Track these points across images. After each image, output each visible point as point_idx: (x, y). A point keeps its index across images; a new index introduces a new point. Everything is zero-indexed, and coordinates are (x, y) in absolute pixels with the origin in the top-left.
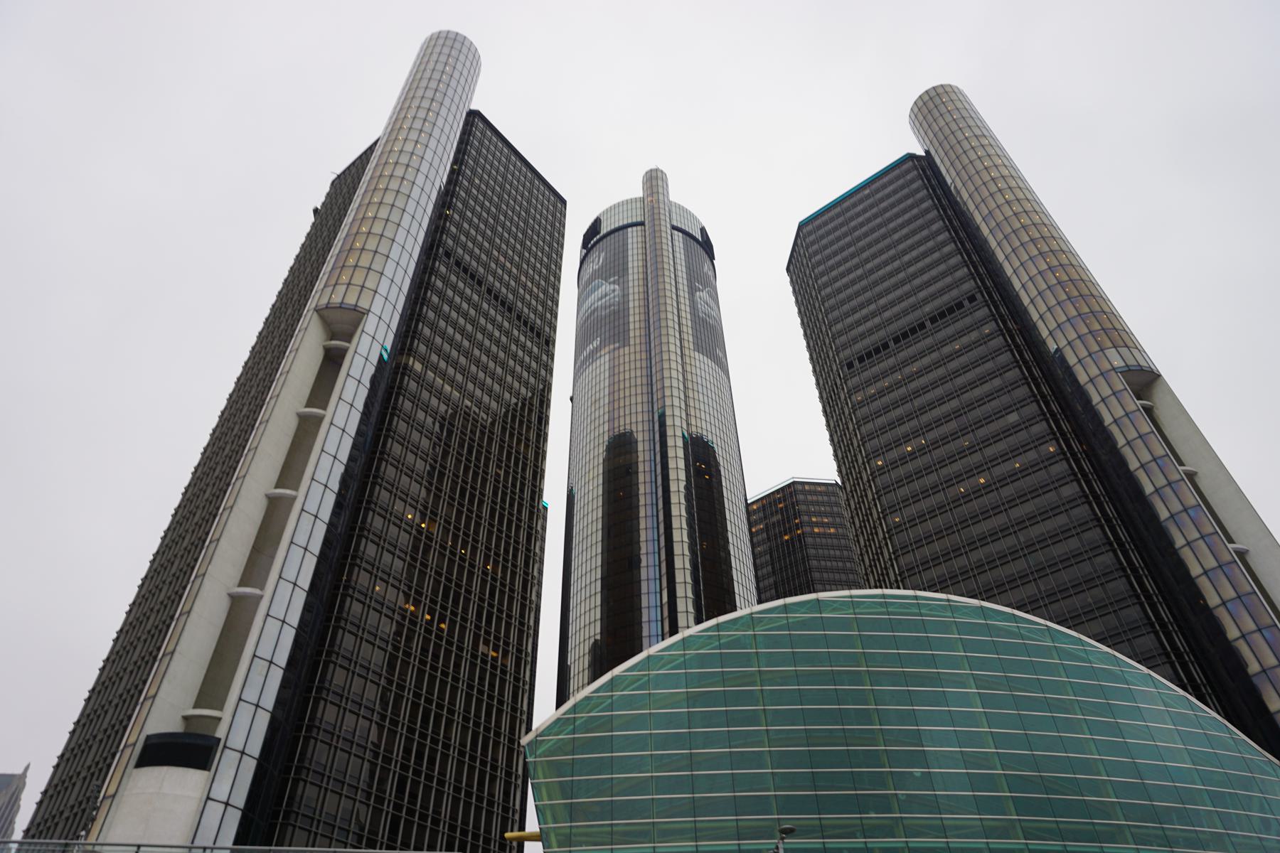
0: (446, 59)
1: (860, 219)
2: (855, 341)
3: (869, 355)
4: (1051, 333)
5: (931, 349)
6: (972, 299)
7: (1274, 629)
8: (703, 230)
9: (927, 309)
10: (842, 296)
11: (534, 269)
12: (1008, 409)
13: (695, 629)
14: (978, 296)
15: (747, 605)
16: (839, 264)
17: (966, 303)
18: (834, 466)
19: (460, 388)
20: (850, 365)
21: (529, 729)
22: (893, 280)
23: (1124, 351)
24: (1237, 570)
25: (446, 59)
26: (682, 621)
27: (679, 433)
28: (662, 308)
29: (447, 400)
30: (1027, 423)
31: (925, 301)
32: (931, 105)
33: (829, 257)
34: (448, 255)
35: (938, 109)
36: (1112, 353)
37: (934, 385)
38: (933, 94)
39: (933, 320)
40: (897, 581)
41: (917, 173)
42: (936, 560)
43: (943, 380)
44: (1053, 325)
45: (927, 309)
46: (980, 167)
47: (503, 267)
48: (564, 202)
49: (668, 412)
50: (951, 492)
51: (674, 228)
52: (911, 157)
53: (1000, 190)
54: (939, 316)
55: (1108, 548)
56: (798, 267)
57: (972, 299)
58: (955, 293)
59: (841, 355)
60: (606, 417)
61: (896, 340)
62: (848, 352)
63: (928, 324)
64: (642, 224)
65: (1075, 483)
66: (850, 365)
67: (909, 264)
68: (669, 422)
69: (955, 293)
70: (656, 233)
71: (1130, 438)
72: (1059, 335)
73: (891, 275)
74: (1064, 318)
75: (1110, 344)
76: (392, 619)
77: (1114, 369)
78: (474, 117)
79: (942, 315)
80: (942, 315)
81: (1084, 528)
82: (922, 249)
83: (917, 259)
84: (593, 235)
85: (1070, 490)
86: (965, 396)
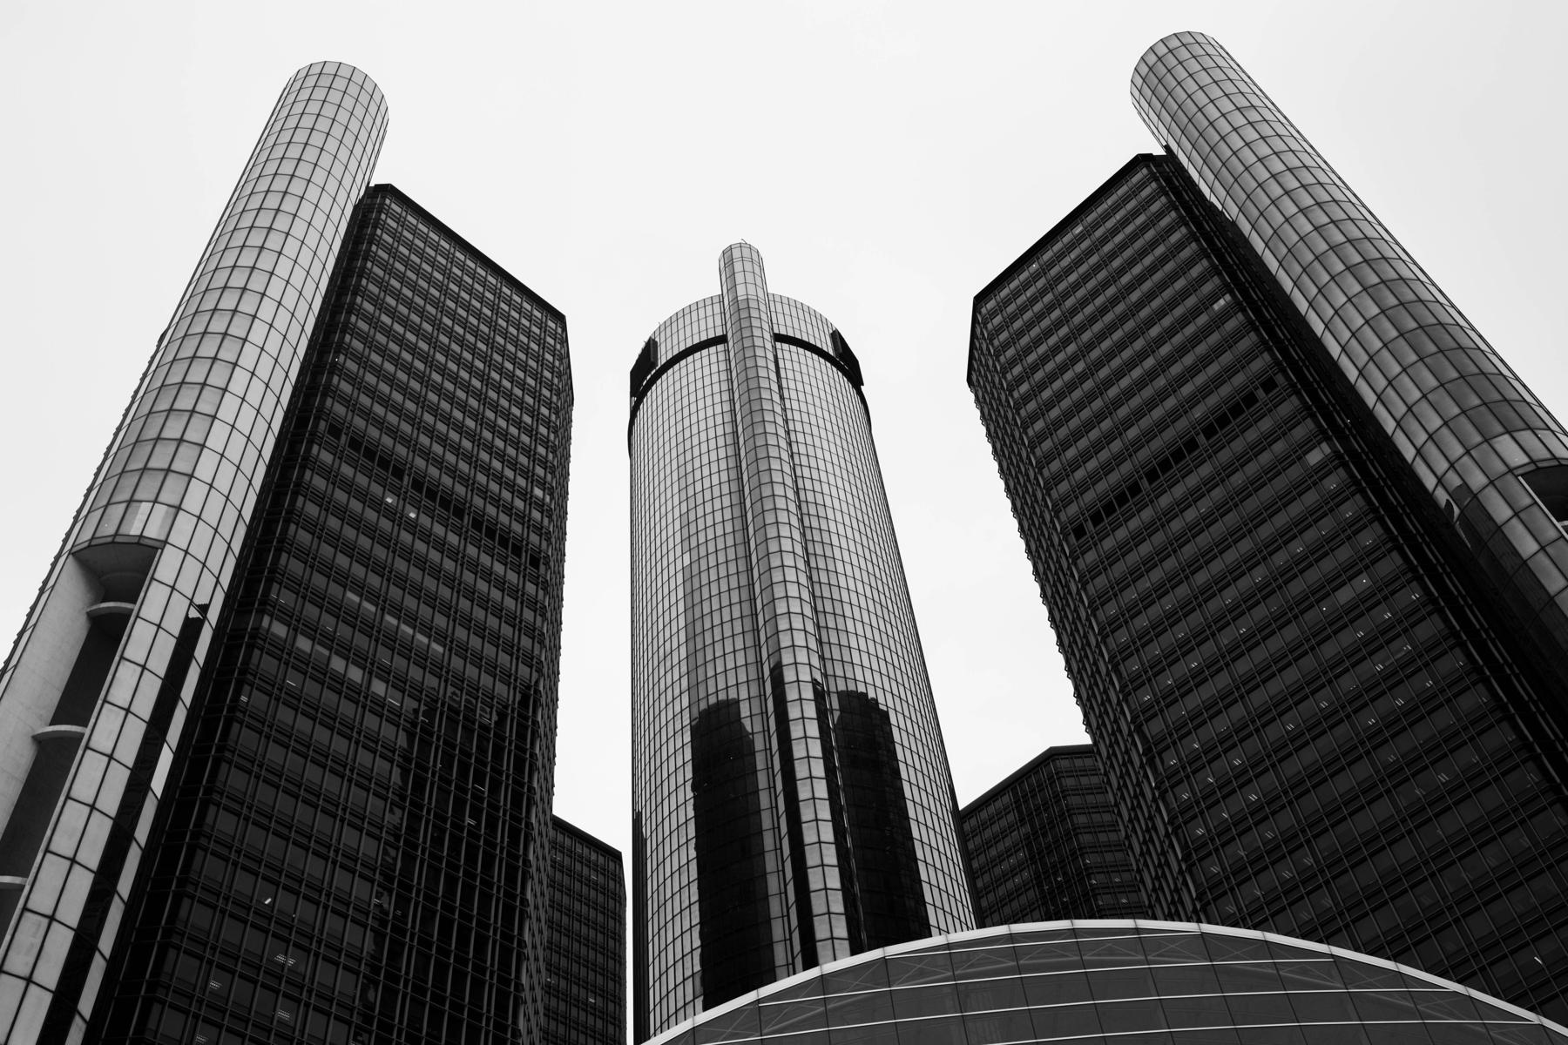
0: (326, 102)
1: (1065, 262)
2: (1083, 487)
3: (1109, 509)
4: (1398, 424)
5: (1209, 485)
6: (1269, 385)
7: (1561, 542)
8: (836, 337)
9: (1198, 412)
10: (1119, 569)
11: (518, 326)
12: (1348, 573)
13: (847, 961)
14: (1280, 379)
15: (952, 927)
16: (1037, 342)
17: (1260, 393)
18: (1077, 713)
19: (442, 637)
20: (1079, 532)
21: (616, 856)
22: (1147, 392)
23: (1526, 437)
24: (1540, 514)
25: (326, 102)
26: (823, 950)
27: (805, 676)
28: (765, 478)
29: (417, 691)
30: (1383, 592)
31: (1193, 401)
32: (1162, 70)
33: (1026, 339)
34: (335, 431)
35: (1174, 74)
36: (1505, 445)
37: (1281, 663)
38: (1162, 50)
39: (1209, 432)
40: (1195, 911)
41: (1154, 176)
42: (1258, 863)
43: (1295, 653)
44: (1401, 409)
45: (1198, 412)
46: (1264, 175)
47: (507, 416)
48: (560, 318)
49: (787, 658)
50: (1273, 732)
51: (779, 338)
52: (1141, 160)
53: (1287, 193)
54: (1217, 425)
55: (1475, 677)
56: (984, 373)
57: (1269, 385)
58: (1239, 379)
59: (1063, 516)
60: (685, 681)
61: (1152, 476)
62: (1073, 509)
63: (1201, 439)
64: (722, 340)
65: (1435, 617)
66: (1079, 532)
67: (1140, 305)
68: (789, 675)
69: (1239, 379)
70: (747, 352)
71: (1391, 375)
72: (1413, 426)
73: (1140, 384)
74: (1438, 422)
75: (1500, 429)
76: (357, 973)
77: (1511, 470)
78: (379, 204)
79: (1223, 421)
80: (1223, 421)
81: (1434, 654)
82: (1190, 330)
83: (1192, 371)
84: (647, 371)
85: (1476, 699)
86: (1309, 616)
